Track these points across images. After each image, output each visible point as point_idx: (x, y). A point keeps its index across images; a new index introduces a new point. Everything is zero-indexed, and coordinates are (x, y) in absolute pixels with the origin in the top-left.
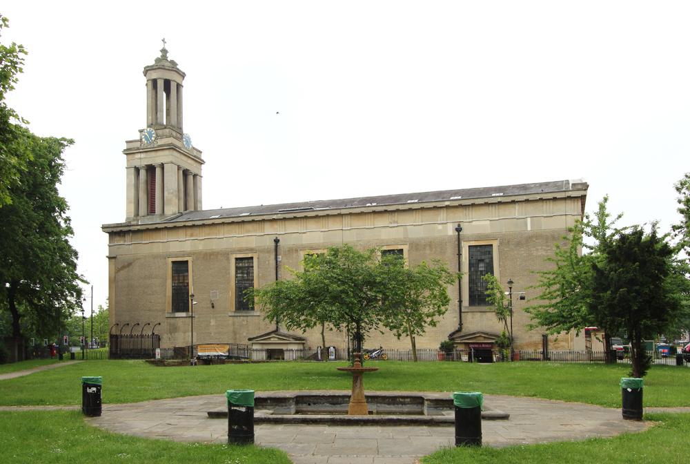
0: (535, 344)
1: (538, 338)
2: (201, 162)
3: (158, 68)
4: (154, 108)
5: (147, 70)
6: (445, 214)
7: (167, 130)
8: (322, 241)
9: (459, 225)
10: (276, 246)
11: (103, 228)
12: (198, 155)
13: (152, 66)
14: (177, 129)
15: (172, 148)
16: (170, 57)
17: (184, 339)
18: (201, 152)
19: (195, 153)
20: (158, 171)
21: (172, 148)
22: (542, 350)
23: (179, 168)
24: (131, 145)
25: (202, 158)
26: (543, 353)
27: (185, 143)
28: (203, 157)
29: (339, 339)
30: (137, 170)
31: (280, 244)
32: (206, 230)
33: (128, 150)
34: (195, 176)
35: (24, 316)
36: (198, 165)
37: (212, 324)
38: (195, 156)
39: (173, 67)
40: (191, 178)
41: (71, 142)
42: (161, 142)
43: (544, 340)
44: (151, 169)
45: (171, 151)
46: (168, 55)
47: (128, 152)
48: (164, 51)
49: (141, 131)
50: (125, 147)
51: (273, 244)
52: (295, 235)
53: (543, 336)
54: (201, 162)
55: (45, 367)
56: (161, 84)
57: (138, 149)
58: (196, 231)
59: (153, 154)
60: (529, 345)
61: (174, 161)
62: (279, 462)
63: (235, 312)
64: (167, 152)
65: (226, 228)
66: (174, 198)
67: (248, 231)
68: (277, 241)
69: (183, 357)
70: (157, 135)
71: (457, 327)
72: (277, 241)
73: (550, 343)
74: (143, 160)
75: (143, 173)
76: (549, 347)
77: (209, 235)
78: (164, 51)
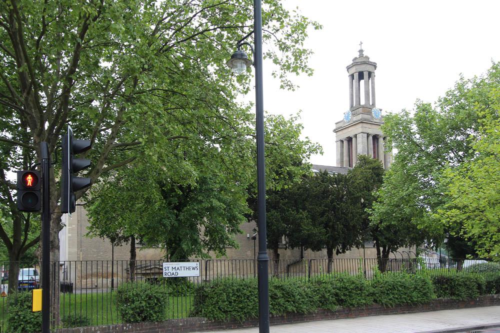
4: (354, 94)
5: (348, 68)
11: (335, 131)
13: (352, 64)
15: (361, 122)
16: (365, 54)
20: (354, 140)
21: (361, 122)
23: (368, 135)
24: (340, 125)
27: (374, 115)
30: (342, 141)
35: (292, 182)
39: (366, 62)
41: (318, 27)
44: (350, 140)
46: (364, 53)
48: (361, 51)
50: (334, 127)
55: (50, 276)
69: (453, 294)
71: (89, 145)
75: (345, 143)
78: (361, 51)
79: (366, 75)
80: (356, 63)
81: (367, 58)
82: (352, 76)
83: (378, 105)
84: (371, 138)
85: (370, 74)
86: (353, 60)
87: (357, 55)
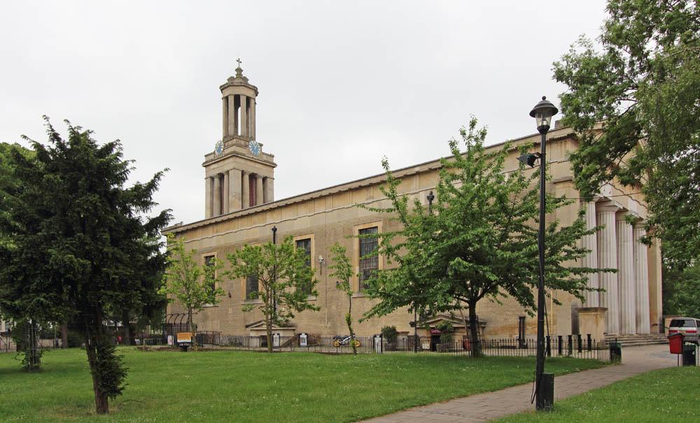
0: (511, 328)
1: (515, 321)
2: (273, 166)
3: (229, 86)
4: (250, 123)
5: (223, 88)
6: (418, 182)
7: (235, 140)
8: (309, 226)
9: (432, 193)
10: (274, 235)
12: (269, 159)
14: (249, 136)
17: (212, 326)
18: (273, 156)
19: (265, 158)
20: (225, 177)
22: (518, 336)
25: (274, 162)
26: (519, 339)
28: (275, 161)
29: (322, 325)
30: (212, 178)
31: (277, 232)
32: (226, 225)
33: (206, 162)
34: (264, 179)
36: (269, 169)
37: (230, 312)
38: (265, 161)
40: (260, 181)
42: (227, 151)
43: (520, 322)
44: (221, 176)
45: (234, 158)
47: (206, 165)
48: (239, 70)
49: (261, 145)
51: (272, 232)
52: (289, 222)
53: (520, 318)
54: (273, 166)
56: (231, 100)
57: (212, 160)
58: (219, 227)
59: (221, 163)
60: (504, 329)
61: (237, 167)
62: (3, 396)
63: (245, 301)
64: (231, 160)
65: (240, 222)
66: (237, 200)
67: (255, 223)
68: (275, 230)
70: (225, 146)
72: (275, 230)
73: (528, 327)
74: (216, 169)
75: (217, 181)
76: (527, 332)
77: (228, 230)
78: (239, 70)
79: (243, 101)
80: (231, 83)
81: (245, 79)
82: (226, 99)
83: (259, 139)
84: (247, 177)
85: (248, 99)
86: (206, 165)
87: (234, 74)
